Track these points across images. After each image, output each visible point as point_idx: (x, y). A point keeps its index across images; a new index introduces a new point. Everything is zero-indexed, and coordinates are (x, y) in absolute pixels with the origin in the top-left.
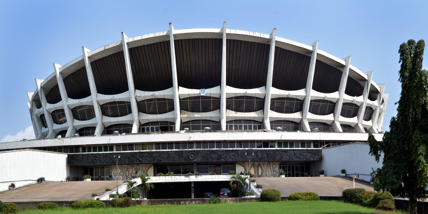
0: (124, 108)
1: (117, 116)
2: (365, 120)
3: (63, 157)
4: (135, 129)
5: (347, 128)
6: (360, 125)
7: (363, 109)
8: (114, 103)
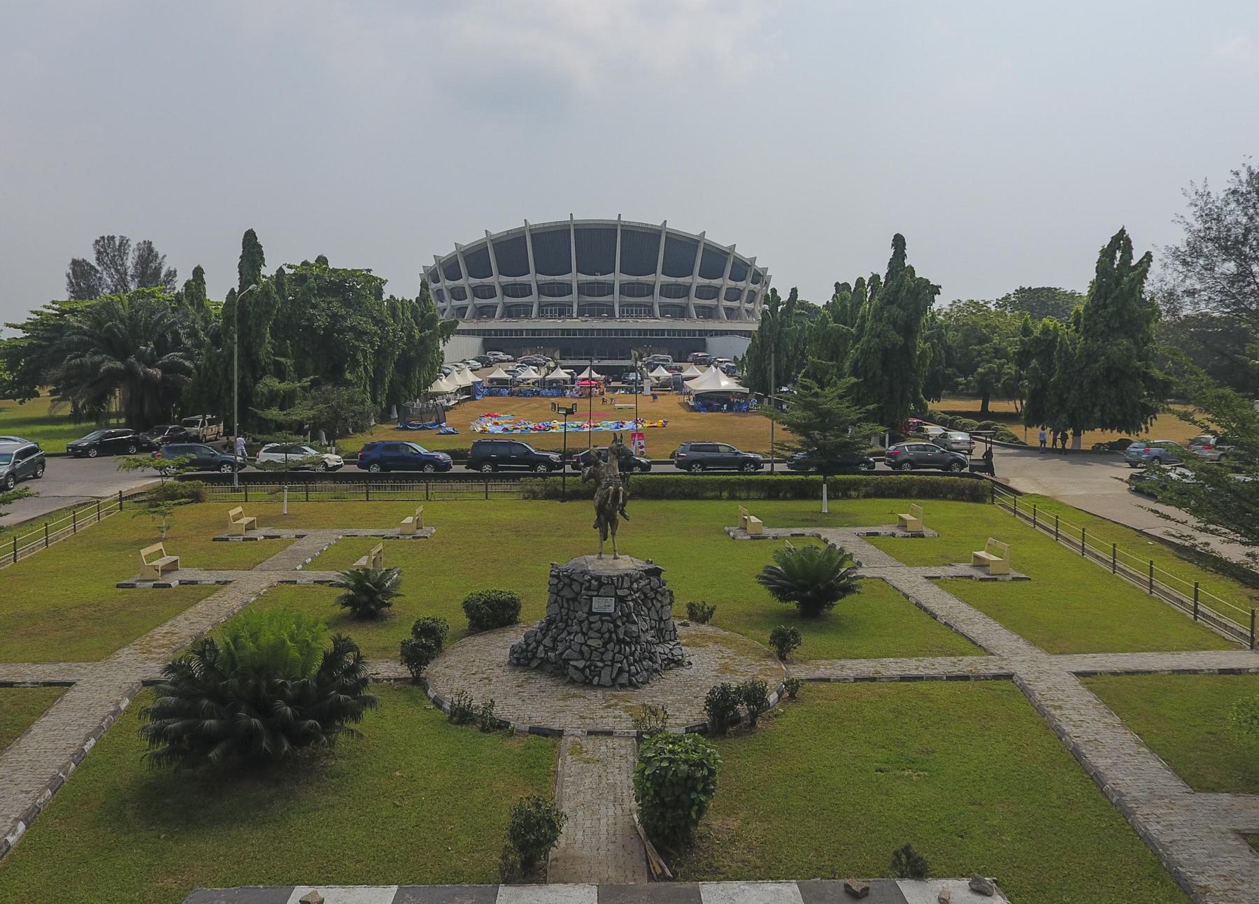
3: (477, 341)
5: (731, 313)
7: (746, 293)
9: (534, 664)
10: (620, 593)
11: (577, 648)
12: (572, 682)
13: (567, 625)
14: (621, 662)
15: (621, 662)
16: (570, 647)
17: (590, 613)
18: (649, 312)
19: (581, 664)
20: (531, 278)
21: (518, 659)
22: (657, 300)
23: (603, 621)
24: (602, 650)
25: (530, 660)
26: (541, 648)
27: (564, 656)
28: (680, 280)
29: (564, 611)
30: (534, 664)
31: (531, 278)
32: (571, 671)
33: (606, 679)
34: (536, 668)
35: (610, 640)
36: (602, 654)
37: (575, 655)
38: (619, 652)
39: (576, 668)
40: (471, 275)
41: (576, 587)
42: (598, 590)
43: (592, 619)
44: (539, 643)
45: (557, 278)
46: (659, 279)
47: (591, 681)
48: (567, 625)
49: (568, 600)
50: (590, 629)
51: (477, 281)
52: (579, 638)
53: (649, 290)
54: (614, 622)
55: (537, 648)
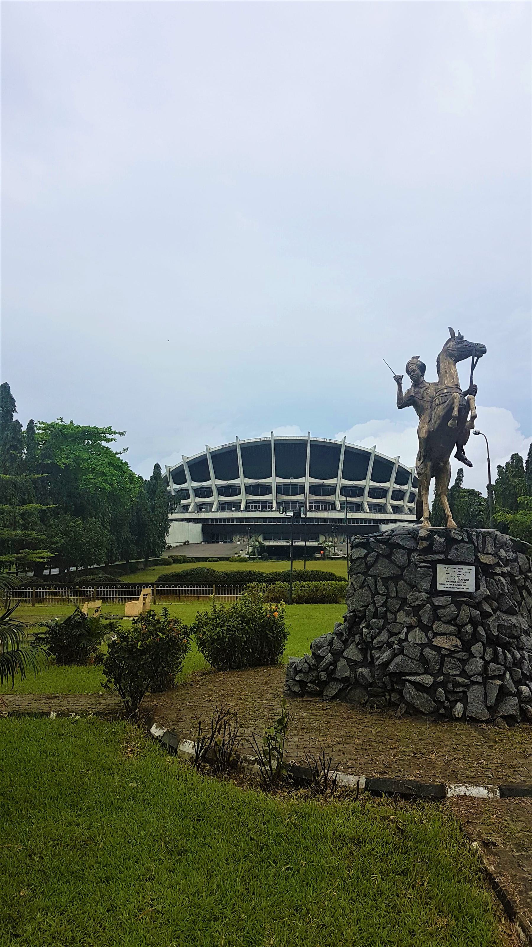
0: (235, 490)
1: (205, 498)
2: (409, 503)
3: (198, 527)
4: (214, 508)
5: (396, 509)
6: (405, 506)
7: (408, 495)
8: (228, 486)
9: (333, 689)
10: (484, 559)
11: (415, 653)
12: (413, 712)
13: (386, 623)
14: (501, 677)
15: (501, 677)
16: (401, 652)
17: (433, 592)
18: (332, 507)
19: (427, 680)
20: (241, 481)
21: (302, 683)
22: (338, 499)
23: (458, 605)
24: (463, 655)
25: (324, 684)
26: (342, 663)
27: (392, 667)
28: (357, 483)
29: (380, 600)
30: (333, 689)
31: (241, 481)
32: (410, 692)
33: (477, 708)
34: (334, 698)
35: (475, 637)
36: (464, 662)
37: (413, 666)
38: (495, 659)
39: (418, 686)
40: (193, 480)
41: (400, 556)
42: (446, 552)
43: (438, 601)
44: (337, 655)
45: (260, 481)
46: (339, 482)
47: (450, 710)
48: (386, 623)
49: (385, 580)
50: (437, 618)
51: (199, 484)
52: (417, 636)
53: (332, 490)
54: (478, 606)
55: (334, 663)
